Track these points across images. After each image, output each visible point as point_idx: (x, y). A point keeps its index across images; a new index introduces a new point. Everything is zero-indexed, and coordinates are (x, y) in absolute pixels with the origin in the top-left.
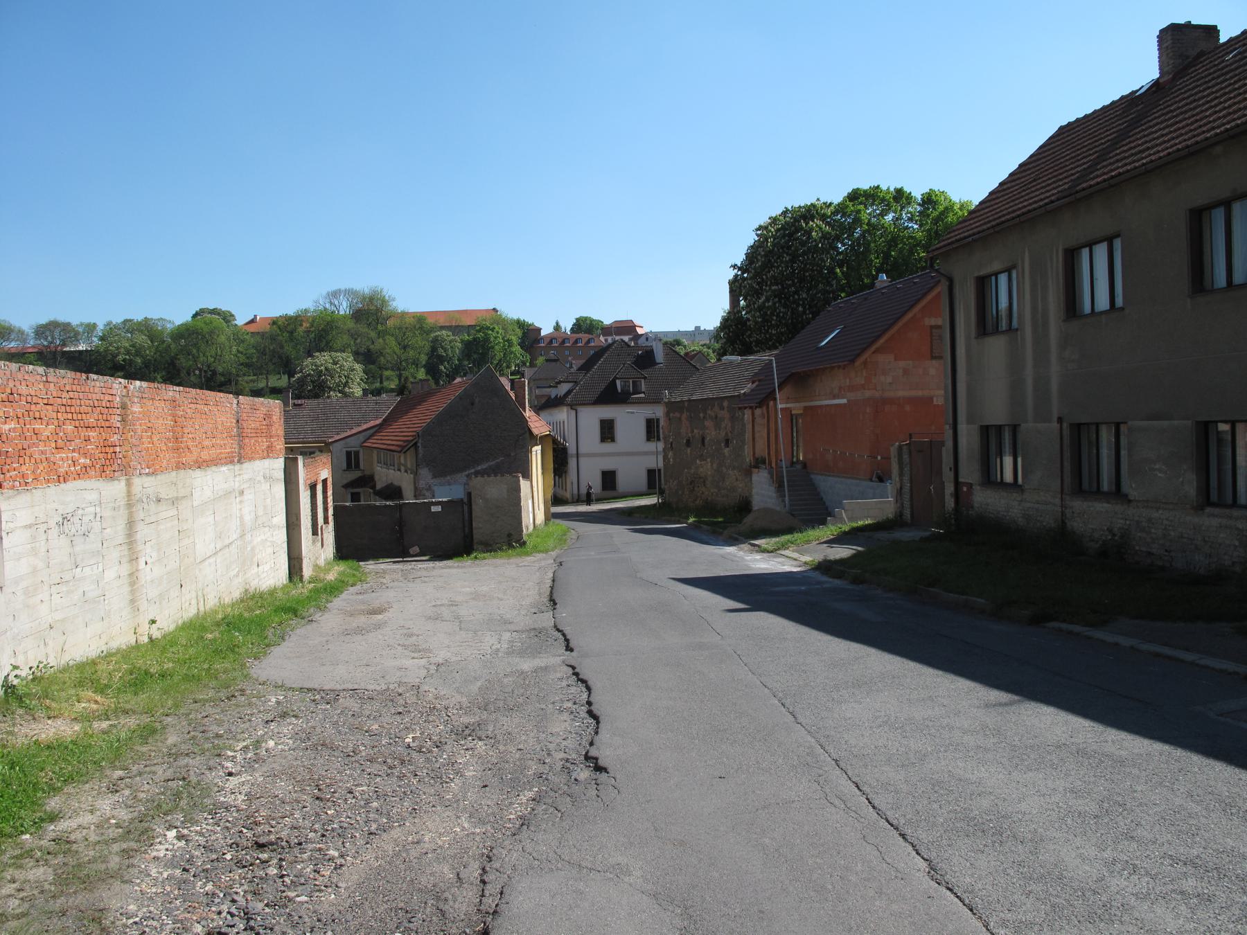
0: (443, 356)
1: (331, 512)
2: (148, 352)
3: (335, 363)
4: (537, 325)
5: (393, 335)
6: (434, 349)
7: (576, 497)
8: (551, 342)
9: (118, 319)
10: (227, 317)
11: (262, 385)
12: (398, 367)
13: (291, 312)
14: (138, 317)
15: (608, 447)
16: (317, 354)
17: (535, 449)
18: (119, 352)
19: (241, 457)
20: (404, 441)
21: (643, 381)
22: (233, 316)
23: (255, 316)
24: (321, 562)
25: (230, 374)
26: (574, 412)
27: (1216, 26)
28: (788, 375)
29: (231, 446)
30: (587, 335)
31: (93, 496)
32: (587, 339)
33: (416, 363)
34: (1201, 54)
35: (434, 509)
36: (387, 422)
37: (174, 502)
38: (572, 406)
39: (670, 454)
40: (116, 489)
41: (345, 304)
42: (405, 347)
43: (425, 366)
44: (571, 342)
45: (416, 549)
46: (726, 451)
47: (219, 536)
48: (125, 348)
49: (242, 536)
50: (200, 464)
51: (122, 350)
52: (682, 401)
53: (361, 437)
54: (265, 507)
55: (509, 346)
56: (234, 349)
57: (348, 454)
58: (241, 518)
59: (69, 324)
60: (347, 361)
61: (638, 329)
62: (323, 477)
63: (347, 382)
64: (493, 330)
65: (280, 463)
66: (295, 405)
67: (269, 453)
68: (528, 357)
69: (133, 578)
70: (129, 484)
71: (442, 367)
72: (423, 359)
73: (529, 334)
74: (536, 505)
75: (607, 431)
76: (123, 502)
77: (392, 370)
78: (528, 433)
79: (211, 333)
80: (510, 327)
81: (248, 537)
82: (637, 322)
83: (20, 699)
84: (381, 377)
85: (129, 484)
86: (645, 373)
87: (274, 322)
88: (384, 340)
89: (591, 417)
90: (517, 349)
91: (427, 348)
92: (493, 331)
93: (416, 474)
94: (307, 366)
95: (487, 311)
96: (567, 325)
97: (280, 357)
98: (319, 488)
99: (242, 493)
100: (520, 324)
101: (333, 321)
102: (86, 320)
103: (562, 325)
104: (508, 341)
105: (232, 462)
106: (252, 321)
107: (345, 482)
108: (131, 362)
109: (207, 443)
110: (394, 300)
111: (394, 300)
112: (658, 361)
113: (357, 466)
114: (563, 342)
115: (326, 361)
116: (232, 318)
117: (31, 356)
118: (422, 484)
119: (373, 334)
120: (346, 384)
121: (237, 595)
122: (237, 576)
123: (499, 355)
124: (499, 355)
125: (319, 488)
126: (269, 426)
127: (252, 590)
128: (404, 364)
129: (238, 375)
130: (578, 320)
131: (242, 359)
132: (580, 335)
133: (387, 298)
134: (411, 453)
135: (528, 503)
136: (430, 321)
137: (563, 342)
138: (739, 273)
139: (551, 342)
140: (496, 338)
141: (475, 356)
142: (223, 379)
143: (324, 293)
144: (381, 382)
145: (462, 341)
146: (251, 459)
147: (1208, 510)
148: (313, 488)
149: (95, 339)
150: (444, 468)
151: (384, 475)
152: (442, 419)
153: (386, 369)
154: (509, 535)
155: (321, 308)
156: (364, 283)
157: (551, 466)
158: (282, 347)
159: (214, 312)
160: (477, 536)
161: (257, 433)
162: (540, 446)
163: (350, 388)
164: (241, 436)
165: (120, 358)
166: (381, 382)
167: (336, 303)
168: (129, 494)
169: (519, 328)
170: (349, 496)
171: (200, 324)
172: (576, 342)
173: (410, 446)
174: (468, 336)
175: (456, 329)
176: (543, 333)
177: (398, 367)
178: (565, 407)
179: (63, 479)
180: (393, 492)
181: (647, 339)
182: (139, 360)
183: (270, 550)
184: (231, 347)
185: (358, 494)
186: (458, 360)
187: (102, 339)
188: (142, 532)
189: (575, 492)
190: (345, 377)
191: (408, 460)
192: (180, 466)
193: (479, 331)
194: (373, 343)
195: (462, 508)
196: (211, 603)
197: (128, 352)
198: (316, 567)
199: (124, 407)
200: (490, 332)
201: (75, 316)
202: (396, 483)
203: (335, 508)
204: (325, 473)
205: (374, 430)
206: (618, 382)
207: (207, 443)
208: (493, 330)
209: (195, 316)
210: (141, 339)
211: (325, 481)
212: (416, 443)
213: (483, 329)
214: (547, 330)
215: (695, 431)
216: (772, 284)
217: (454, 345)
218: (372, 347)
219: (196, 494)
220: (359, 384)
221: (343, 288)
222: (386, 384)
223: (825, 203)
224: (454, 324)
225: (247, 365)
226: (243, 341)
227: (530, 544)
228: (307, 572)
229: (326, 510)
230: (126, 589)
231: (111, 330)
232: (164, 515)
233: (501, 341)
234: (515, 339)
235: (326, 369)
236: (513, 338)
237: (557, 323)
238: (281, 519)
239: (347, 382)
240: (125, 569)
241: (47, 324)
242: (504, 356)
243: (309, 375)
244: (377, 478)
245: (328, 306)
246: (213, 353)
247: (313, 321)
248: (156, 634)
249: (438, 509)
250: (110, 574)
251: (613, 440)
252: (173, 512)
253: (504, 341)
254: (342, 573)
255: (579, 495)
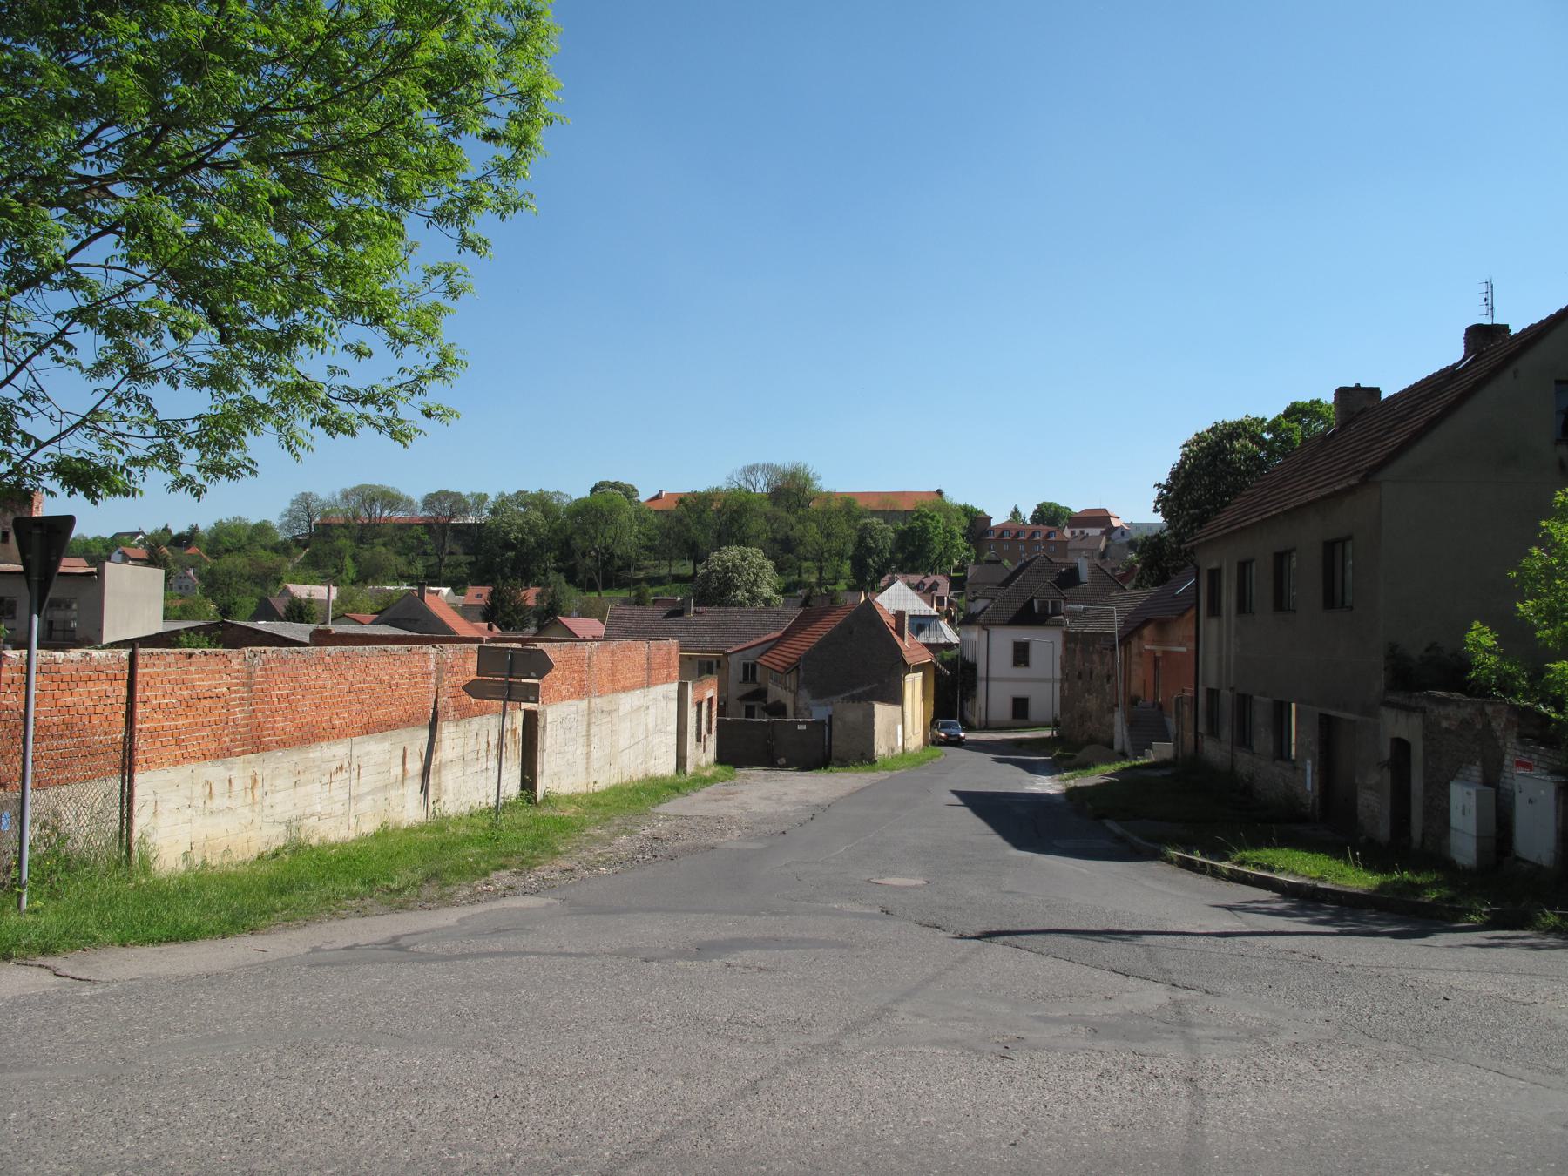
0: (871, 548)
1: (714, 724)
2: (541, 530)
3: (744, 559)
4: (988, 513)
5: (814, 521)
6: (862, 539)
7: (983, 724)
8: (1002, 534)
9: (510, 491)
10: (629, 492)
11: (664, 571)
12: (819, 558)
13: (701, 488)
14: (533, 488)
15: (1021, 672)
16: (725, 548)
17: (909, 677)
18: (512, 530)
19: (649, 683)
20: (789, 663)
21: (1063, 601)
22: (636, 490)
23: (661, 491)
24: (703, 763)
25: (630, 557)
26: (985, 633)
27: (1507, 326)
28: (1142, 620)
29: (643, 676)
30: (1046, 527)
31: (574, 708)
32: (1046, 532)
33: (840, 555)
34: (1363, 411)
35: (800, 727)
36: (787, 635)
37: (610, 713)
38: (984, 626)
39: (1066, 685)
40: (583, 705)
41: (762, 482)
42: (828, 536)
43: (850, 558)
44: (1027, 536)
45: (782, 761)
46: (1107, 686)
47: (633, 736)
48: (518, 525)
49: (647, 737)
50: (625, 689)
51: (515, 527)
52: (1077, 633)
53: (759, 650)
54: (663, 718)
55: (952, 538)
56: (636, 529)
57: (746, 666)
58: (647, 725)
59: (459, 494)
60: (756, 556)
61: (1112, 519)
62: (708, 696)
63: (756, 580)
64: (932, 518)
65: (675, 686)
66: (695, 612)
67: (668, 679)
68: (974, 552)
69: (588, 754)
70: (589, 702)
71: (870, 561)
72: (850, 549)
73: (976, 523)
74: (909, 730)
75: (1021, 654)
76: (586, 713)
77: (813, 560)
78: (901, 664)
79: (611, 511)
80: (954, 515)
81: (650, 738)
82: (1111, 512)
83: (549, 801)
84: (800, 568)
85: (589, 702)
86: (1066, 593)
87: (682, 500)
88: (805, 527)
89: (1004, 639)
90: (960, 542)
91: (855, 535)
92: (933, 520)
93: (796, 694)
94: (713, 561)
95: (929, 493)
96: (1027, 512)
97: (686, 542)
98: (705, 705)
99: (648, 708)
100: (967, 511)
101: (748, 502)
102: (477, 491)
103: (1021, 510)
104: (950, 532)
105: (643, 687)
106: (657, 497)
107: (741, 694)
108: (523, 541)
109: (629, 675)
110: (819, 478)
111: (819, 478)
112: (1082, 580)
113: (754, 679)
114: (1017, 535)
115: (734, 556)
116: (634, 493)
117: (419, 528)
118: (801, 704)
119: (792, 519)
120: (754, 583)
121: (641, 776)
122: (642, 764)
123: (939, 548)
124: (939, 548)
125: (705, 705)
126: (669, 660)
127: (650, 775)
128: (826, 555)
129: (638, 560)
130: (1039, 506)
131: (644, 541)
132: (1041, 526)
133: (811, 476)
134: (794, 674)
135: (896, 729)
136: (861, 504)
137: (1017, 535)
138: (1165, 492)
139: (1002, 534)
140: (936, 528)
141: (911, 548)
142: (621, 563)
143: (740, 468)
144: (799, 576)
145: (895, 531)
146: (655, 684)
147: (1278, 762)
148: (699, 705)
149: (485, 512)
150: (822, 691)
151: (776, 693)
152: (821, 646)
153: (806, 560)
154: (862, 754)
155: (735, 486)
156: (784, 459)
157: (931, 692)
158: (688, 530)
159: (615, 485)
160: (834, 754)
161: (661, 666)
162: (921, 674)
163: (758, 587)
164: (649, 669)
165: (512, 536)
166: (799, 576)
167: (753, 479)
168: (589, 708)
169: (966, 515)
170: (744, 711)
171: (600, 501)
172: (1033, 535)
173: (794, 667)
174: (904, 525)
175: (889, 515)
176: (994, 523)
177: (819, 558)
178: (977, 628)
179: (563, 699)
180: (779, 709)
181: (1123, 534)
182: (532, 539)
183: (664, 750)
184: (631, 527)
185: (753, 707)
186: (890, 553)
187: (493, 512)
188: (594, 729)
189: (983, 717)
190: (754, 574)
191: (791, 681)
192: (614, 691)
193: (917, 519)
194: (792, 529)
195: (821, 728)
196: (626, 778)
197: (521, 530)
198: (698, 766)
199: (589, 658)
200: (929, 521)
201: (464, 485)
202: (783, 701)
203: (718, 721)
204: (711, 692)
205: (772, 643)
206: (1036, 603)
207: (629, 675)
208: (932, 518)
209: (593, 491)
210: (536, 515)
211: (710, 699)
212: (797, 667)
213: (922, 516)
214: (999, 517)
215: (1086, 664)
216: (1191, 508)
217: (887, 534)
218: (790, 533)
219: (621, 708)
220: (769, 583)
221: (761, 463)
222: (805, 576)
223: (1256, 419)
224: (889, 509)
225: (648, 548)
226: (645, 520)
227: (879, 763)
228: (690, 768)
229: (710, 722)
230: (585, 761)
231: (504, 503)
232: (604, 720)
233: (942, 532)
234: (958, 530)
235: (734, 565)
236: (956, 529)
237: (1016, 509)
238: (673, 727)
239: (756, 580)
240: (585, 750)
241: (436, 494)
242: (945, 550)
243: (714, 571)
244: (769, 693)
245: (743, 483)
246: (612, 533)
247: (725, 501)
248: (597, 790)
249: (804, 727)
250: (579, 752)
251: (1027, 664)
252: (609, 719)
253: (946, 532)
254: (715, 773)
255: (987, 722)
